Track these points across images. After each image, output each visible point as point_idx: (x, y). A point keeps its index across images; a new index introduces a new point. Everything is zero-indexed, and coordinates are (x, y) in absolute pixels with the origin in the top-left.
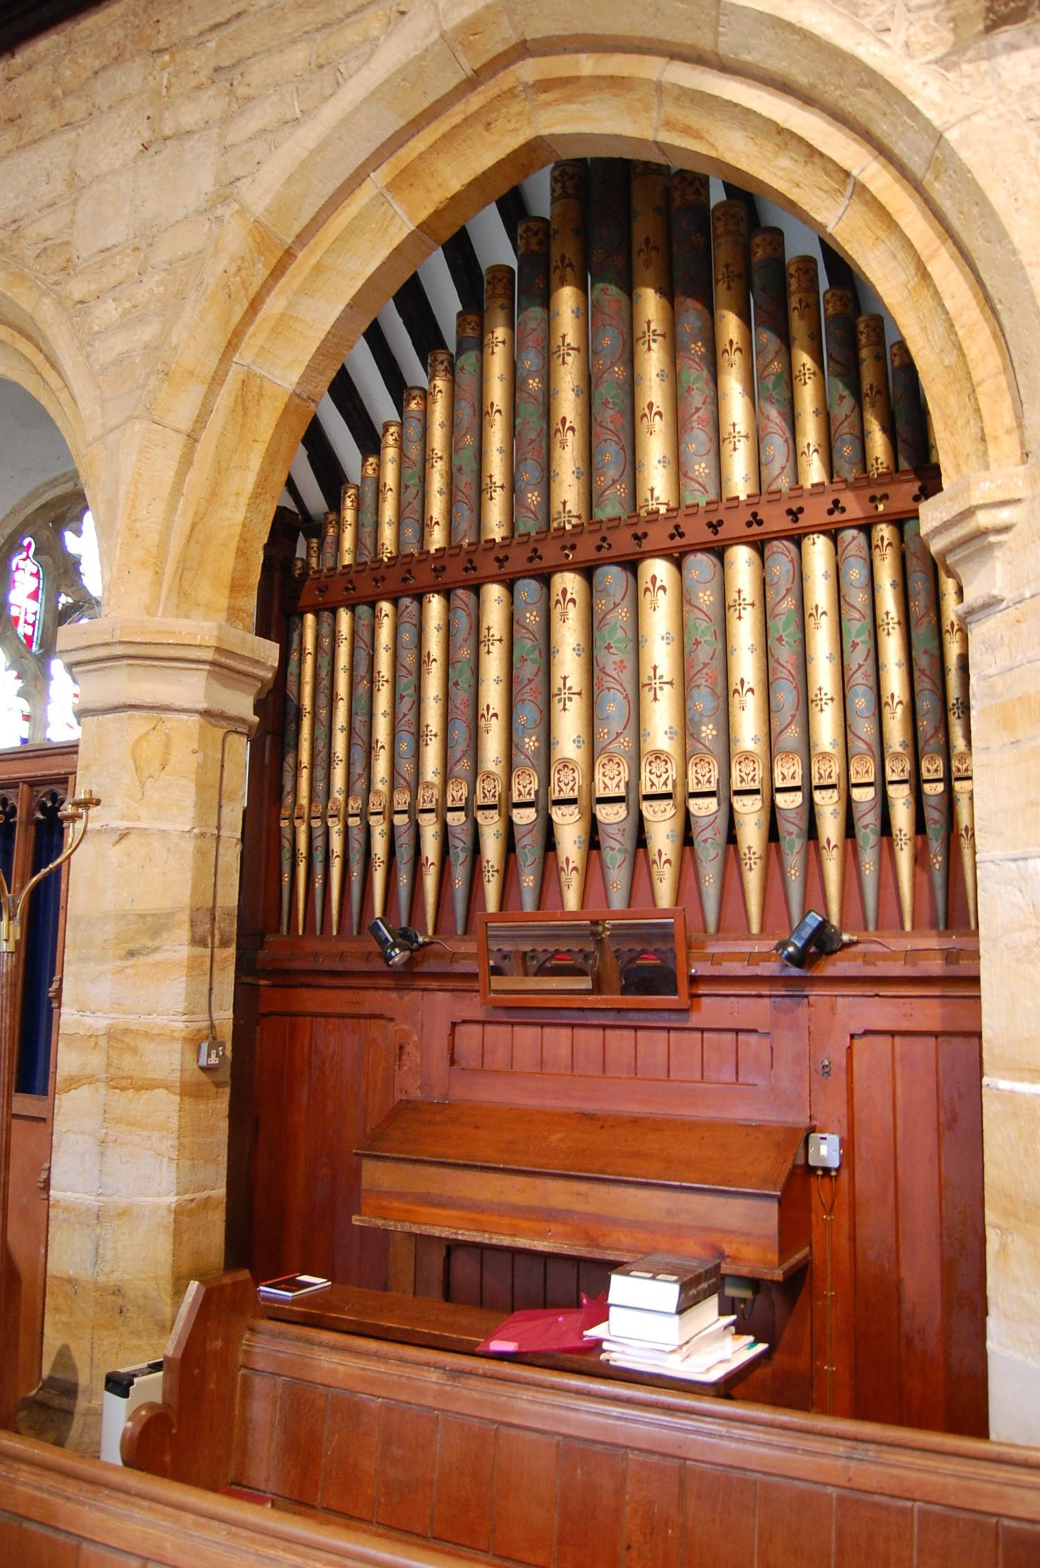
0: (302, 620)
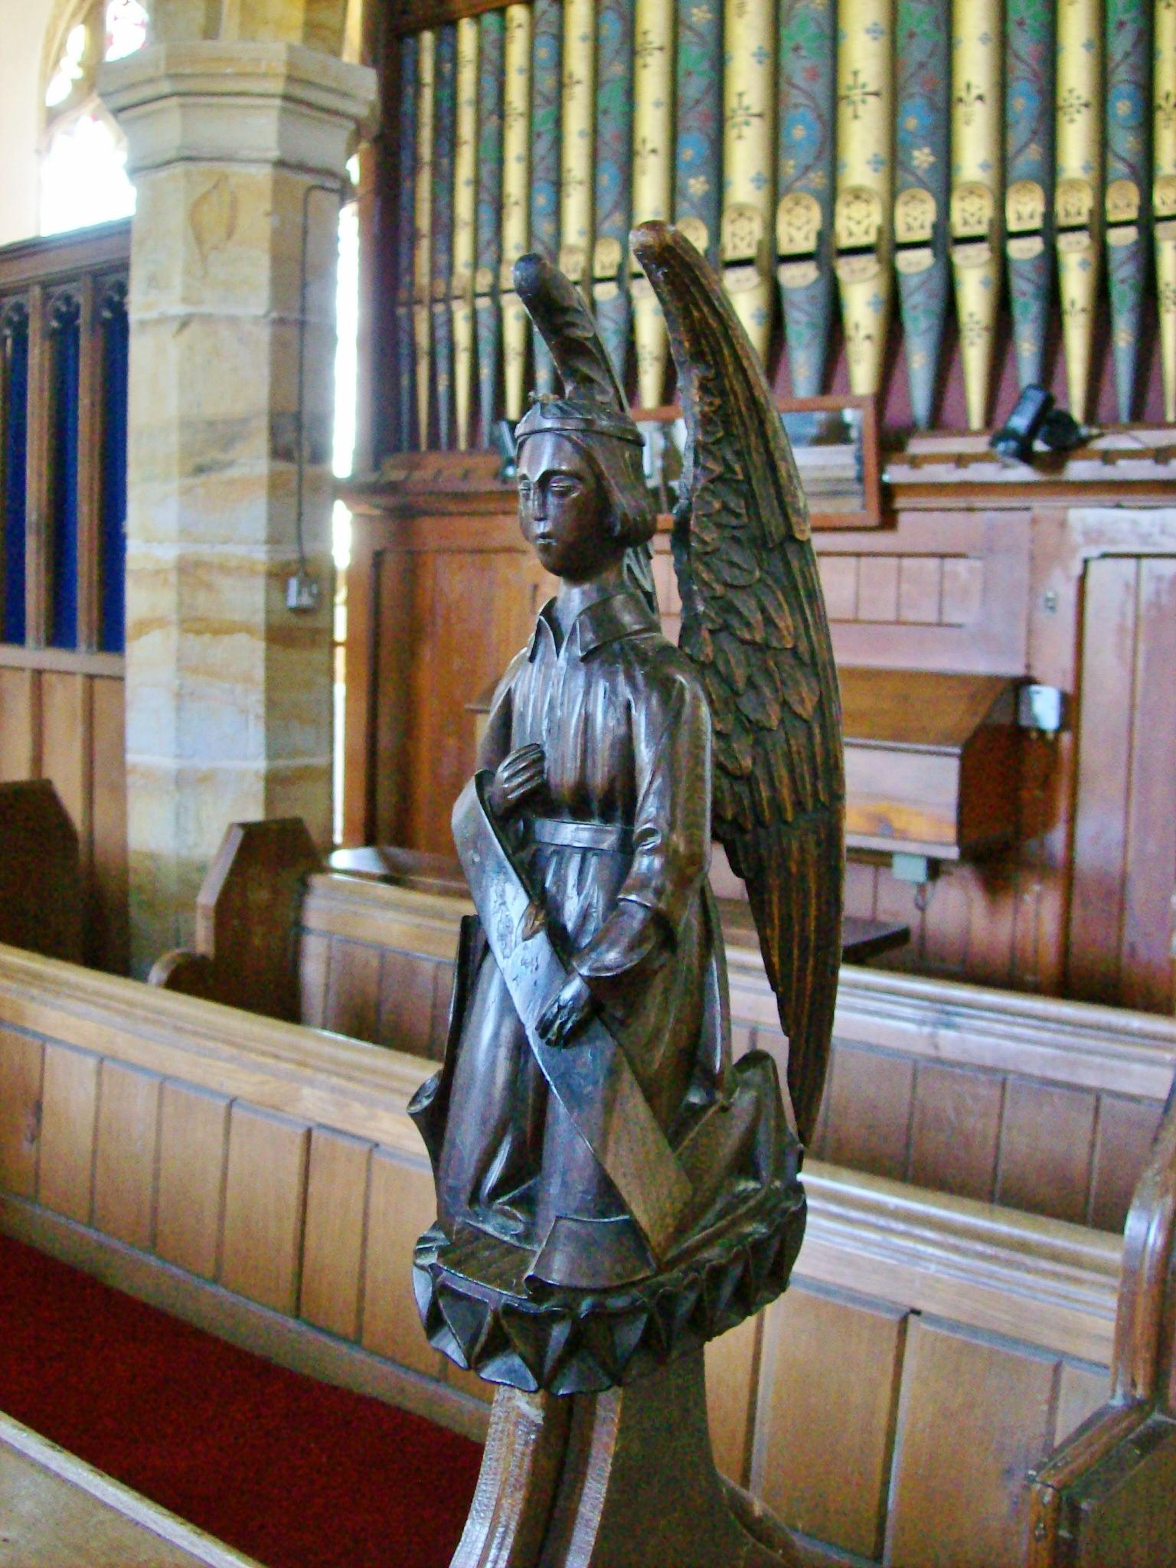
0: (418, 40)
